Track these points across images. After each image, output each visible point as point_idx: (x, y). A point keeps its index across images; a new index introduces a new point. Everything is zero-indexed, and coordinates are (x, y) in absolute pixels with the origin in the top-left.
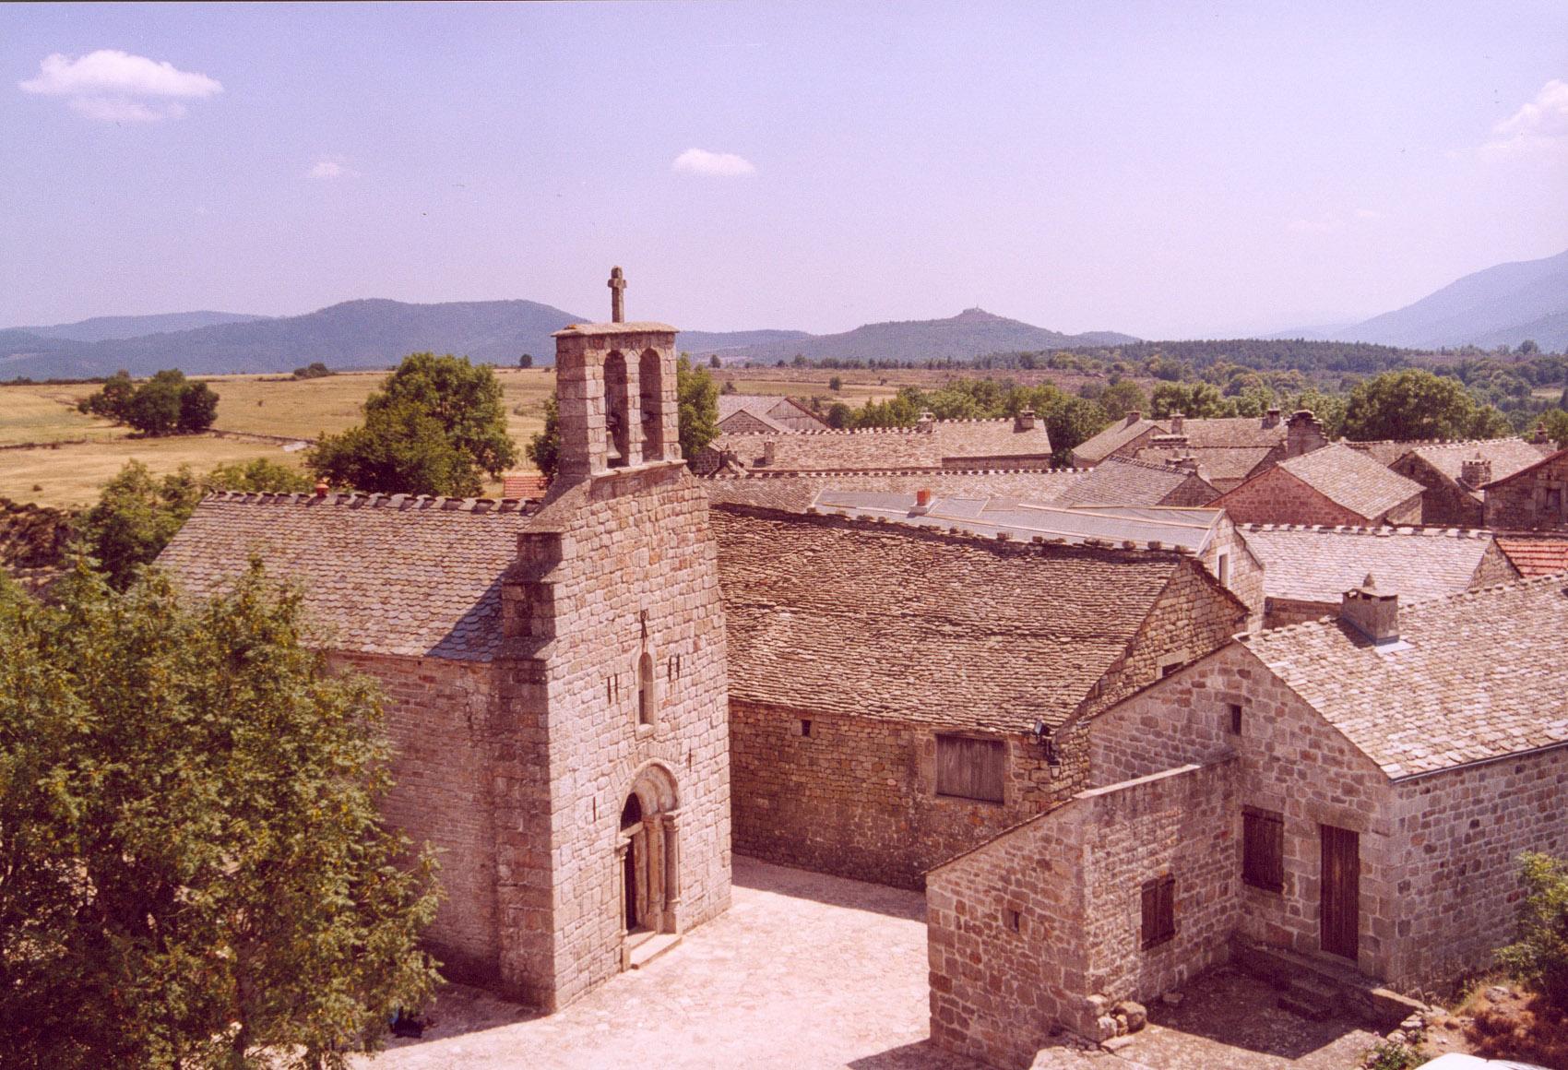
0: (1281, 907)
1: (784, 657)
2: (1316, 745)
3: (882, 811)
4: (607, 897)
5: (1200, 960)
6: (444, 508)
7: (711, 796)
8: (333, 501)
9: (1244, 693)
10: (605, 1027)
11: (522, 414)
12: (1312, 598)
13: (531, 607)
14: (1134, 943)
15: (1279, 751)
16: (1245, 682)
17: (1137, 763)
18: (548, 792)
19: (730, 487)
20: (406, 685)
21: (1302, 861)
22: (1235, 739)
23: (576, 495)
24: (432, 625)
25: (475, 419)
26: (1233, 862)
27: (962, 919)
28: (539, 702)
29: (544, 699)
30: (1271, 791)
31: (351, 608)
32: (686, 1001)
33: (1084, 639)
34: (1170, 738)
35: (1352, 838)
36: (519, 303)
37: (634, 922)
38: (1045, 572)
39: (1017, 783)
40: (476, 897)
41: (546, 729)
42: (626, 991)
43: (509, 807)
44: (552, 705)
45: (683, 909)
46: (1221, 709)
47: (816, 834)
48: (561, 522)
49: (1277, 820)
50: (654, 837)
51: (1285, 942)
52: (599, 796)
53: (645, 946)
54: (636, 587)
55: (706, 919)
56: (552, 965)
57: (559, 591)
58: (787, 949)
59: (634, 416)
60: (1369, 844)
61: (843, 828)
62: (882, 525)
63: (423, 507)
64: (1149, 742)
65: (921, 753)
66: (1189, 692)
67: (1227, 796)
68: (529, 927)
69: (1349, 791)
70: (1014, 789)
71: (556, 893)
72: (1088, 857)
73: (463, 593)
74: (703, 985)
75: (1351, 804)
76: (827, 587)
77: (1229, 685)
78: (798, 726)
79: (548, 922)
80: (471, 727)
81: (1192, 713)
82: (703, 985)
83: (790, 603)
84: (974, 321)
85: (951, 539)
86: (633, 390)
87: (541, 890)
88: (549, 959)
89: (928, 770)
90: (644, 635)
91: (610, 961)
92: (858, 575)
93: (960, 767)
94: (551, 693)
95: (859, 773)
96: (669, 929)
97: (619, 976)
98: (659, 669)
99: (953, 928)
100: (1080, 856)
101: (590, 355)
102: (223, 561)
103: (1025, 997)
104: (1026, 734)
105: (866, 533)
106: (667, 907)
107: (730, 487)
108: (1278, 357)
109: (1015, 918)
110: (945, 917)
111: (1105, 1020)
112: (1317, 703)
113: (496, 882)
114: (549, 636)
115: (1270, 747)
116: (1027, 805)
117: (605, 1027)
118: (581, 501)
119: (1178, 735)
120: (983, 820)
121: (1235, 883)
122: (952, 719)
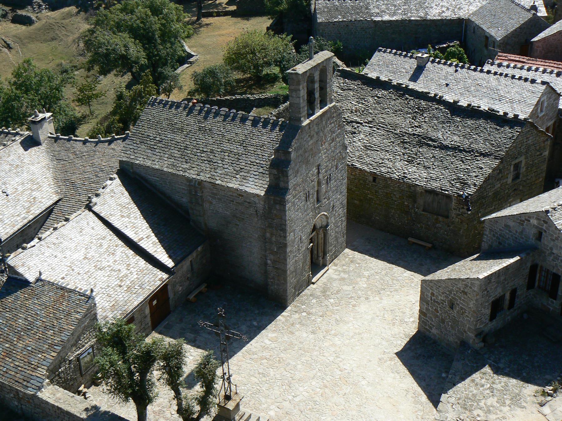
9: (544, 228)
15: (555, 251)
16: (545, 225)
17: (501, 238)
18: (286, 240)
20: (232, 196)
22: (539, 243)
24: (241, 174)
27: (433, 298)
34: (514, 234)
39: (454, 212)
42: (311, 295)
56: (287, 293)
58: (366, 273)
64: (506, 233)
66: (524, 221)
68: (278, 280)
70: (453, 214)
76: (384, 116)
77: (539, 224)
78: (371, 179)
80: (257, 214)
81: (524, 229)
87: (283, 270)
89: (421, 201)
90: (319, 173)
95: (394, 199)
99: (429, 299)
109: (452, 306)
113: (266, 264)
115: (551, 249)
116: (457, 220)
117: (304, 314)
119: (517, 234)
120: (440, 222)
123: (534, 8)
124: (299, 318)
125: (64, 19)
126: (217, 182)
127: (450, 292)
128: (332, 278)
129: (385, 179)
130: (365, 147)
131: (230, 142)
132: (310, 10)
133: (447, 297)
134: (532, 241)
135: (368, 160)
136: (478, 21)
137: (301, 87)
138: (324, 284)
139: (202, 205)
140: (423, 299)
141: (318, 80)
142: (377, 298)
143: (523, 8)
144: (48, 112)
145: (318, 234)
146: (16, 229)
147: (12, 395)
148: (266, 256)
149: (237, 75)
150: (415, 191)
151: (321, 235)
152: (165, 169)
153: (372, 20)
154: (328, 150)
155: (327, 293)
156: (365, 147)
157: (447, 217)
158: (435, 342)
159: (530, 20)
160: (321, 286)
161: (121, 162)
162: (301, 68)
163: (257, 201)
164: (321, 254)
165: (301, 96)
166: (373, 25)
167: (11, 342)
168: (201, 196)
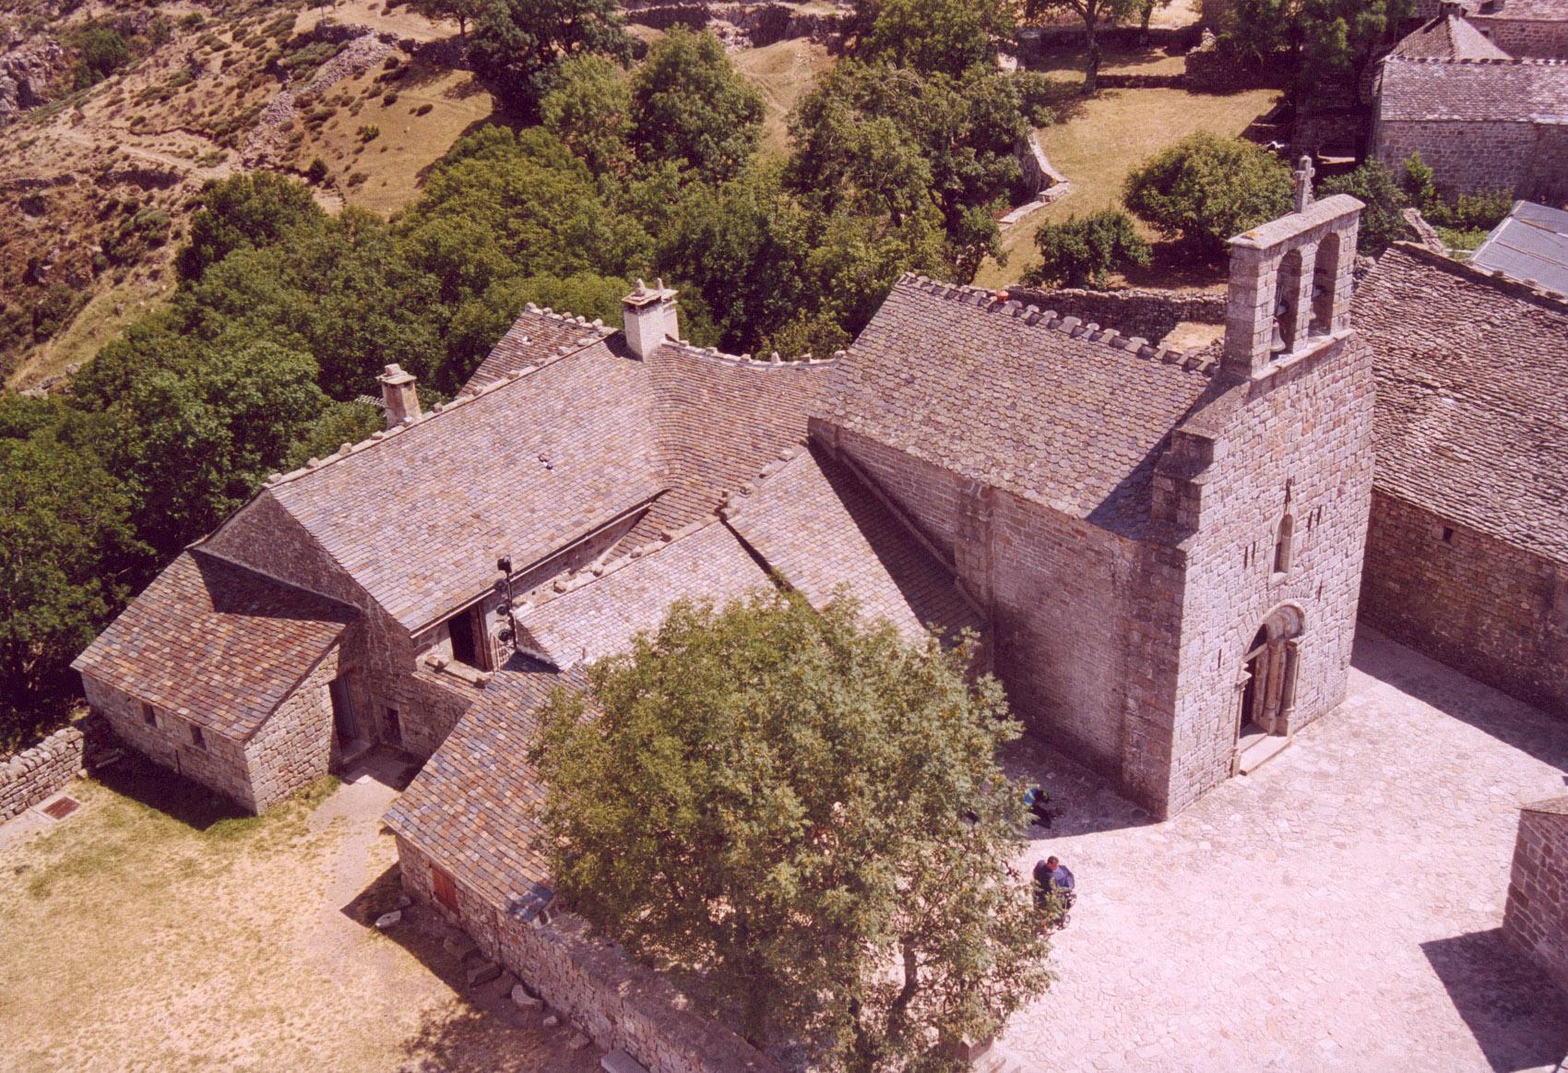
1: (1438, 451)
3: (1512, 628)
4: (1223, 724)
6: (1112, 344)
7: (1338, 616)
10: (1205, 845)
13: (1178, 500)
19: (1441, 73)
23: (1234, 396)
24: (1088, 480)
27: (1548, 860)
29: (1182, 583)
31: (1019, 443)
32: (1283, 825)
37: (1250, 723)
40: (1107, 712)
41: (1181, 607)
42: (1230, 802)
43: (1141, 657)
44: (1188, 587)
45: (1294, 715)
47: (1442, 628)
48: (1216, 427)
50: (1276, 658)
52: (1225, 647)
53: (1257, 749)
54: (1286, 460)
55: (1318, 716)
57: (1205, 491)
58: (1389, 771)
59: (1304, 306)
63: (1092, 338)
71: (1176, 734)
73: (1117, 463)
76: (1499, 375)
78: (1439, 531)
79: (1167, 754)
83: (1456, 388)
86: (1306, 281)
88: (1164, 780)
90: (1288, 499)
91: (1221, 772)
92: (1534, 365)
94: (1188, 577)
95: (1494, 589)
96: (1280, 732)
97: (1228, 782)
101: (1264, 267)
102: (911, 359)
105: (1553, 315)
106: (1281, 713)
107: (1441, 73)
110: (1533, 851)
113: (1124, 708)
114: (1191, 529)
117: (1205, 845)
118: (1238, 404)
124: (1191, 855)
125: (773, 70)
126: (1027, 495)
129: (1476, 536)
130: (1436, 449)
131: (1074, 401)
137: (1260, 281)
138: (1274, 780)
139: (986, 545)
140: (1521, 859)
141: (1312, 266)
142: (1404, 838)
144: (666, 286)
146: (556, 545)
147: (483, 918)
149: (1145, 233)
150: (1552, 576)
152: (910, 450)
153: (1531, 122)
155: (1275, 804)
156: (1436, 449)
158: (1543, 974)
160: (1262, 785)
161: (812, 421)
163: (1117, 552)
165: (1259, 302)
166: (1531, 136)
167: (498, 799)
168: (988, 524)
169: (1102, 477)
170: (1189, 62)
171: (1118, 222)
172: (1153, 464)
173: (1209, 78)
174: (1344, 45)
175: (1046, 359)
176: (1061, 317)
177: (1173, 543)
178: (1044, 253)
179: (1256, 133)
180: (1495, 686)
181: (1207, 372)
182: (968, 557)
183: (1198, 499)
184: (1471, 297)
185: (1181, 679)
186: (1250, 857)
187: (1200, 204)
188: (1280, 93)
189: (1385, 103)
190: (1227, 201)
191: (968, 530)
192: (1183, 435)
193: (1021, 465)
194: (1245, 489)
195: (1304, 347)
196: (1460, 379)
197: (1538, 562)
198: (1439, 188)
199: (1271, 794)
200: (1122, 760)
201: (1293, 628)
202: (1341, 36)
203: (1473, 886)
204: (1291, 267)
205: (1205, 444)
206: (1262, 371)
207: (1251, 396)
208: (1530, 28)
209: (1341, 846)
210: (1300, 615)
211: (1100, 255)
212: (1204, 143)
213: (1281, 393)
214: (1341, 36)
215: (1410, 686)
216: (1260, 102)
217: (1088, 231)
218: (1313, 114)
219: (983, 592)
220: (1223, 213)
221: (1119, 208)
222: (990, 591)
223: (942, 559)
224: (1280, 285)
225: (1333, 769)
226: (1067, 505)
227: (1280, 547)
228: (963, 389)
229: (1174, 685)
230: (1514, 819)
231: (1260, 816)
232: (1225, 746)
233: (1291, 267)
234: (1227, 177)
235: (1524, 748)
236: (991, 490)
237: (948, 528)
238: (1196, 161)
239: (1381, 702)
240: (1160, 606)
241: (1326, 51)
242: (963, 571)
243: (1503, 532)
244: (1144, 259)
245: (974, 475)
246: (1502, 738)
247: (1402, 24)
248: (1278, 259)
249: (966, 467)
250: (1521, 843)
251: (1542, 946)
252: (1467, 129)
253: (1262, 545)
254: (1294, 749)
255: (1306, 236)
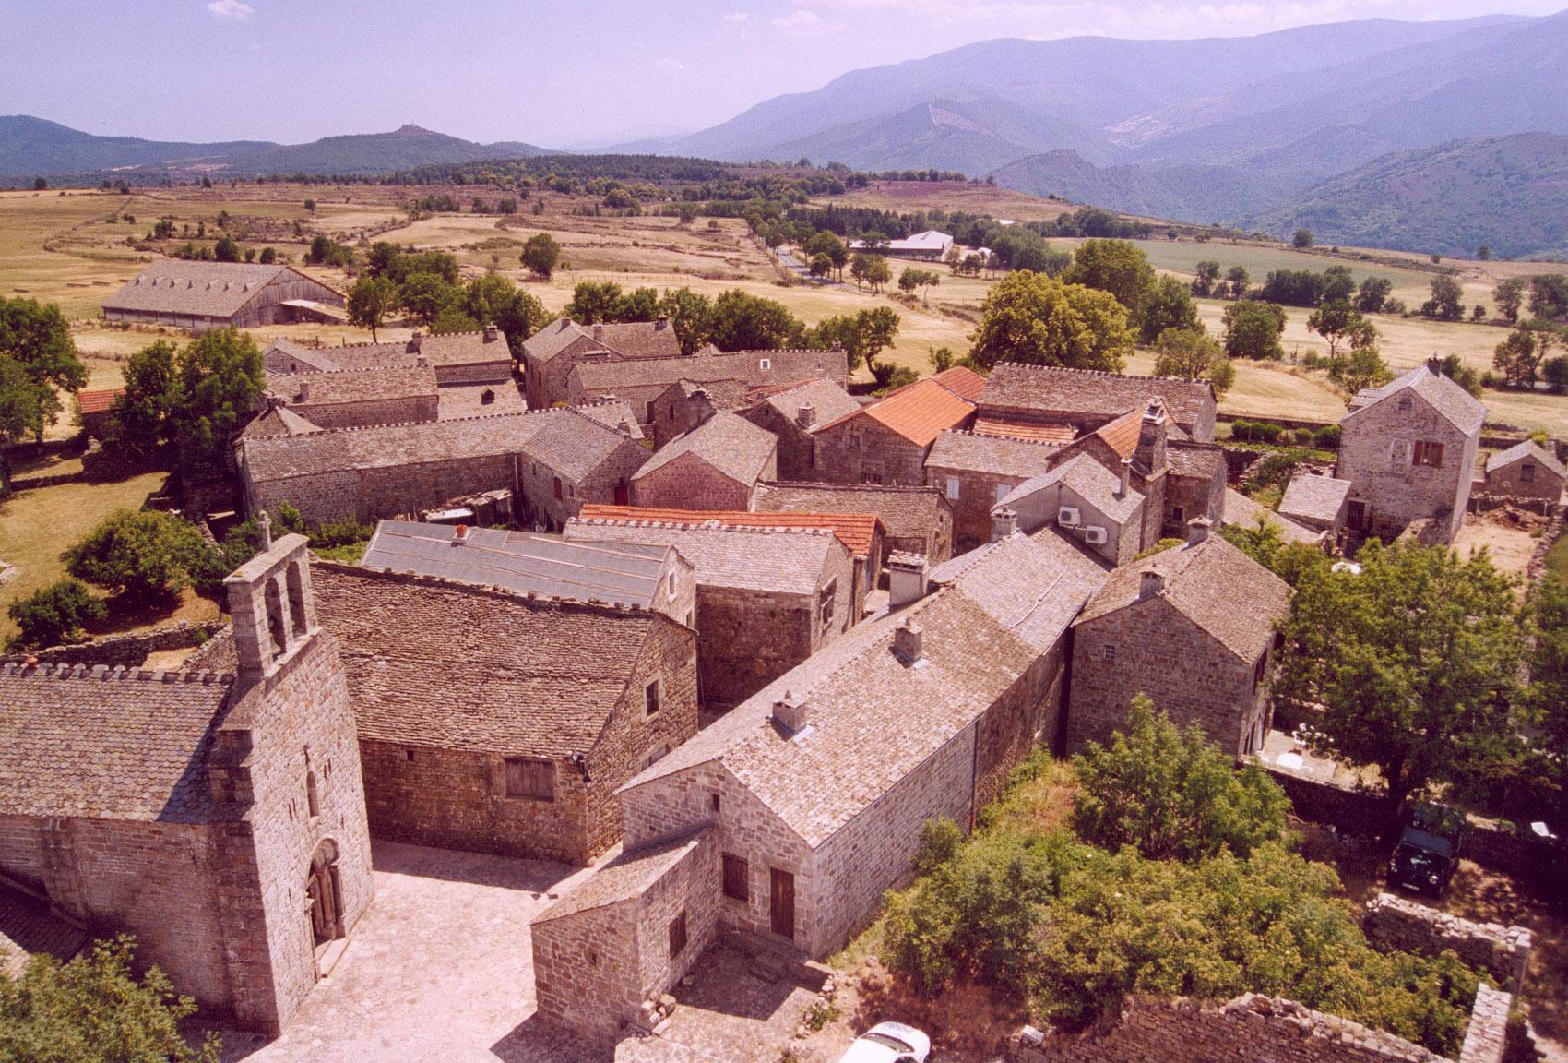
0: (747, 909)
2: (767, 823)
5: (700, 948)
8: (44, 672)
10: (317, 1042)
11: (50, 250)
12: (726, 584)
14: (665, 959)
15: (744, 824)
21: (759, 886)
25: (50, 352)
26: (717, 884)
28: (250, 846)
29: (252, 846)
30: (739, 846)
31: (83, 776)
32: (367, 1003)
33: (596, 680)
35: (791, 877)
36: (21, 118)
37: (320, 938)
38: (564, 624)
43: (232, 914)
44: (258, 848)
46: (706, 796)
48: (249, 720)
49: (745, 862)
51: (749, 929)
55: (362, 914)
57: (253, 771)
59: (286, 616)
60: (799, 881)
61: (443, 818)
62: (442, 584)
63: (121, 678)
65: (495, 770)
67: (712, 849)
69: (788, 851)
70: (560, 792)
71: (273, 964)
72: (640, 927)
73: (173, 764)
74: (376, 985)
75: (789, 858)
76: (410, 637)
78: (404, 755)
79: (270, 983)
82: (376, 985)
83: (384, 653)
84: (412, 137)
85: (494, 596)
86: (284, 599)
88: (272, 1005)
89: (501, 780)
90: (308, 760)
91: (309, 981)
93: (522, 776)
94: (256, 840)
96: (340, 935)
98: (319, 776)
100: (635, 928)
101: (254, 594)
103: (601, 999)
104: (567, 759)
105: (432, 590)
108: (638, 169)
111: (655, 1016)
112: (766, 800)
113: (225, 959)
114: (249, 802)
115: (738, 821)
117: (317, 1042)
121: (719, 895)
122: (515, 749)
123: (624, 427)
126: (103, 815)
127: (586, 935)
128: (358, 959)
129: (430, 751)
130: (385, 698)
132: (235, 460)
133: (581, 946)
134: (705, 814)
135: (392, 722)
136: (537, 454)
137: (255, 605)
138: (348, 972)
139: (74, 868)
140: (538, 960)
142: (452, 978)
143: (606, 428)
145: (319, 879)
148: (222, 944)
151: (327, 879)
154: (318, 716)
156: (385, 698)
157: (551, 799)
158: (573, 1033)
159: (622, 447)
162: (251, 571)
164: (330, 917)
166: (357, 478)
168: (71, 850)
169: (163, 783)
170: (85, 462)
171: (73, 589)
172: (203, 762)
173: (103, 471)
174: (209, 435)
175: (87, 702)
176: (89, 668)
177: (237, 818)
178: (19, 624)
179: (153, 503)
180: (467, 850)
181: (223, 682)
182: (59, 884)
183: (249, 778)
184: (375, 589)
185: (268, 920)
186: (353, 1037)
187: (135, 561)
188: (165, 474)
189: (253, 470)
190: (154, 557)
191: (54, 861)
192: (224, 733)
193: (90, 792)
194: (279, 762)
195: (293, 648)
196: (385, 646)
197: (476, 756)
198: (307, 522)
199: (350, 984)
200: (233, 1002)
201: (330, 855)
202: (207, 428)
203: (507, 993)
204: (272, 592)
205: (243, 736)
206: (271, 671)
207: (267, 691)
208: (330, 409)
209: (413, 1002)
210: (333, 843)
211: (69, 616)
212: (125, 518)
213: (290, 679)
214: (207, 428)
215: (416, 870)
216: (153, 482)
217: (54, 598)
218: (195, 486)
219: (80, 909)
220: (154, 567)
221: (70, 579)
222: (85, 905)
223: (31, 893)
224: (267, 603)
225: (386, 948)
226: (142, 813)
227: (311, 797)
228: (17, 745)
229: (263, 927)
230: (529, 929)
231: (349, 1003)
232: (307, 960)
233: (272, 592)
234: (150, 540)
235: (501, 885)
236: (68, 822)
237: (33, 865)
238: (124, 533)
239: (400, 887)
240: (240, 868)
241: (197, 441)
242: (57, 896)
243: (447, 743)
244: (102, 613)
245: (50, 813)
246: (486, 883)
247: (243, 415)
248: (263, 587)
249: (40, 809)
250: (536, 948)
251: (568, 1014)
252: (313, 479)
253: (298, 800)
254: (354, 943)
255: (277, 567)
